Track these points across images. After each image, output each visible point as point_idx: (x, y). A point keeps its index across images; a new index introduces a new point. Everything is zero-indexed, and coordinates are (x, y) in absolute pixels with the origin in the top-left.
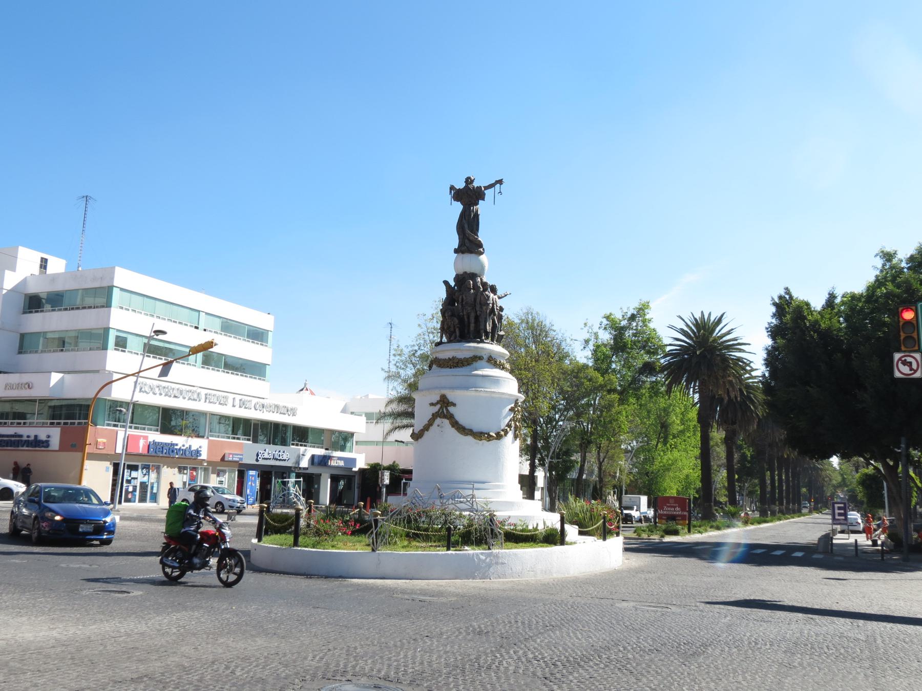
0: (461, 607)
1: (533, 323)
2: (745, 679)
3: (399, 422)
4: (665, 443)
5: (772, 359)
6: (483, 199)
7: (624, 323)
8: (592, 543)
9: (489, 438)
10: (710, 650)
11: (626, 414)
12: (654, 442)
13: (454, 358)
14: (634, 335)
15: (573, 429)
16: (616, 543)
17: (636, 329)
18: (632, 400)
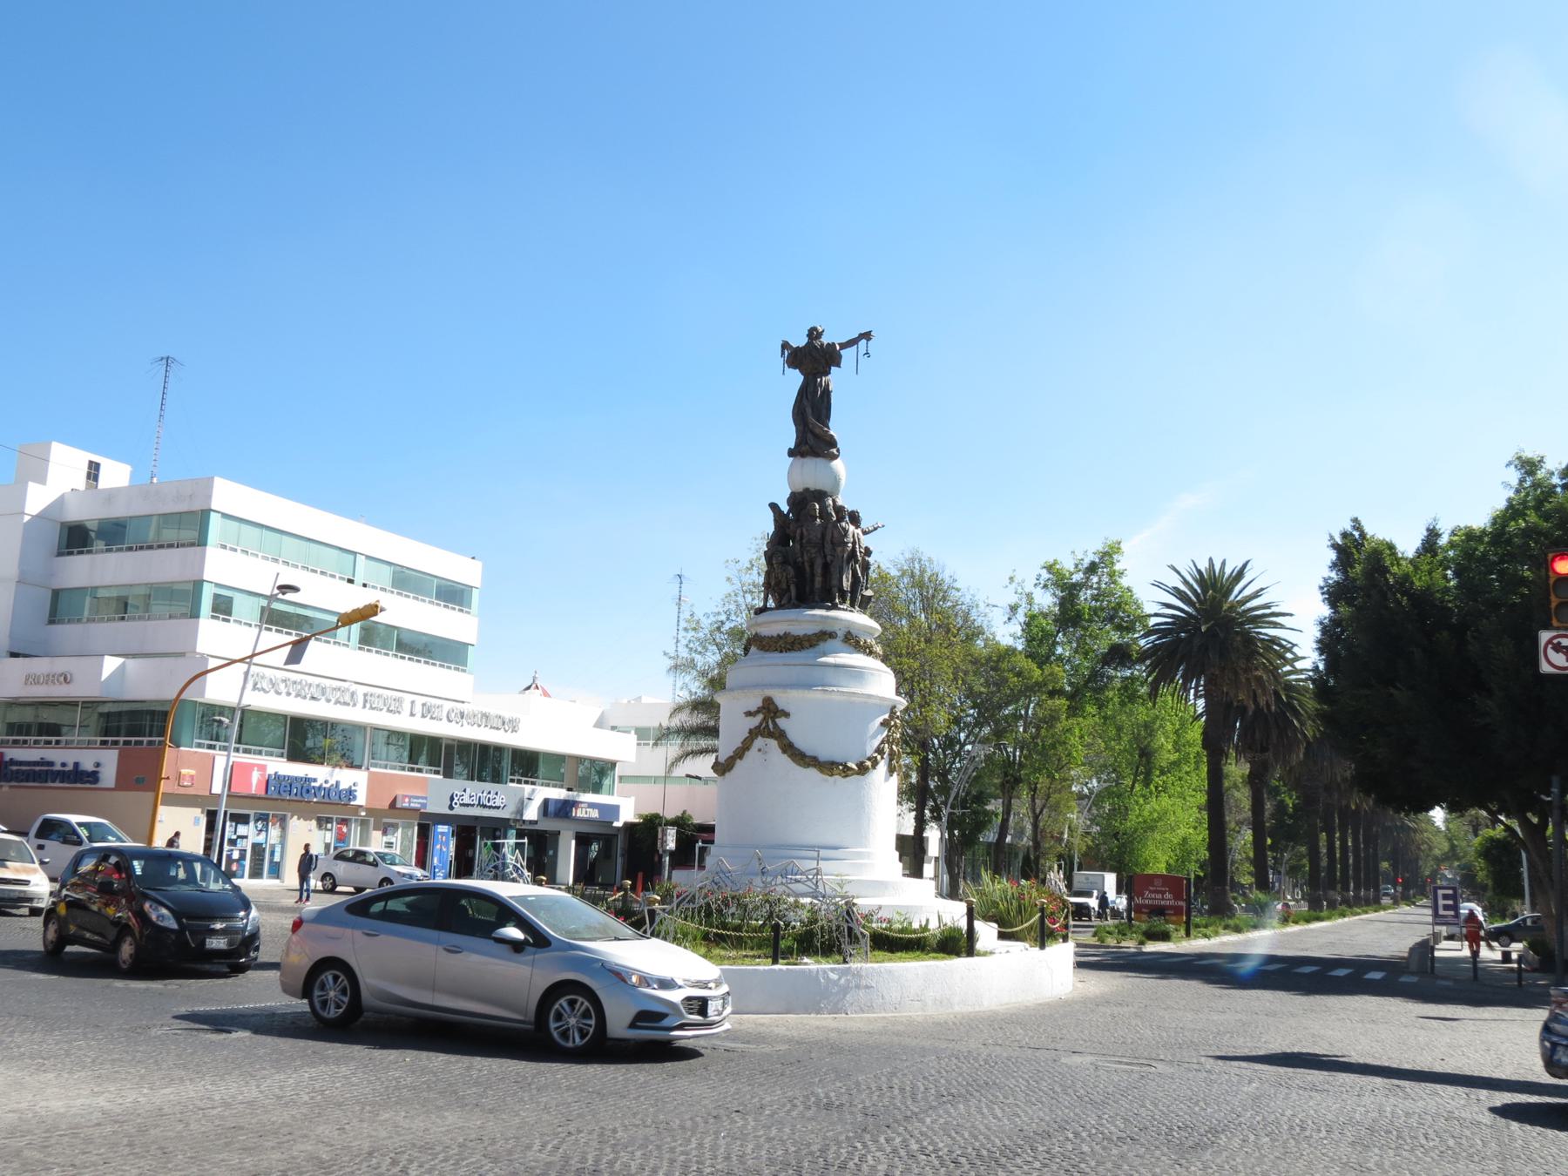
5: (1329, 641)
6: (838, 365)
7: (1078, 577)
9: (847, 771)
11: (1080, 734)
12: (1128, 782)
13: (786, 635)
14: (1095, 598)
15: (989, 758)
16: (1062, 953)
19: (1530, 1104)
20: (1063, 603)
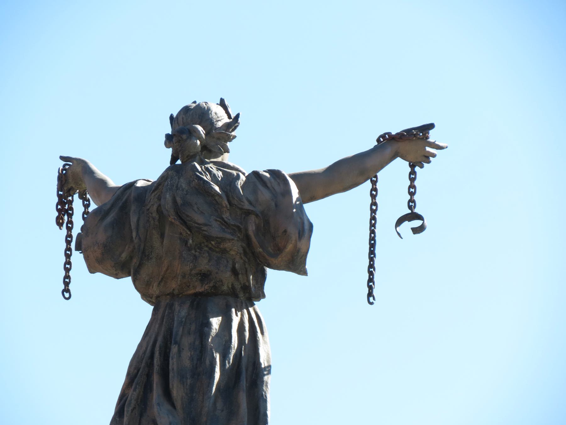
6: (296, 264)
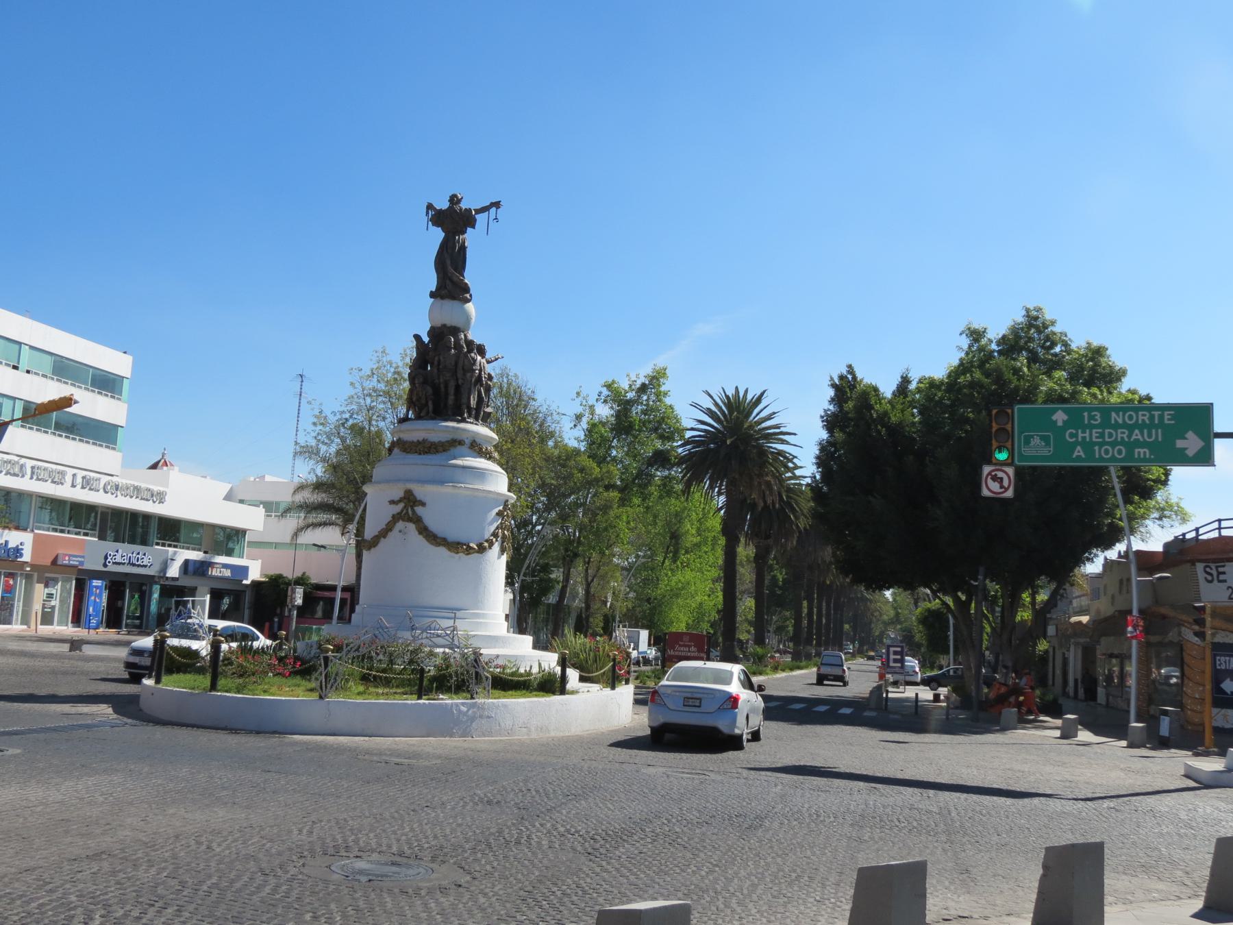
0: (450, 771)
1: (509, 388)
2: (814, 854)
3: (323, 517)
4: (675, 560)
5: (826, 457)
7: (630, 395)
8: (595, 692)
9: (469, 550)
10: (767, 823)
11: (627, 521)
12: (660, 558)
13: (424, 441)
14: (644, 412)
15: (556, 537)
16: (626, 692)
17: (647, 405)
18: (636, 501)
19: (655, 909)
20: (618, 415)
